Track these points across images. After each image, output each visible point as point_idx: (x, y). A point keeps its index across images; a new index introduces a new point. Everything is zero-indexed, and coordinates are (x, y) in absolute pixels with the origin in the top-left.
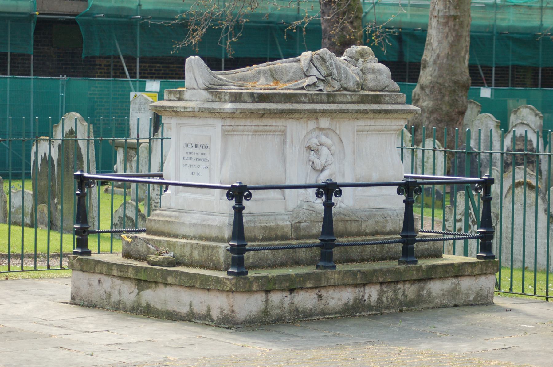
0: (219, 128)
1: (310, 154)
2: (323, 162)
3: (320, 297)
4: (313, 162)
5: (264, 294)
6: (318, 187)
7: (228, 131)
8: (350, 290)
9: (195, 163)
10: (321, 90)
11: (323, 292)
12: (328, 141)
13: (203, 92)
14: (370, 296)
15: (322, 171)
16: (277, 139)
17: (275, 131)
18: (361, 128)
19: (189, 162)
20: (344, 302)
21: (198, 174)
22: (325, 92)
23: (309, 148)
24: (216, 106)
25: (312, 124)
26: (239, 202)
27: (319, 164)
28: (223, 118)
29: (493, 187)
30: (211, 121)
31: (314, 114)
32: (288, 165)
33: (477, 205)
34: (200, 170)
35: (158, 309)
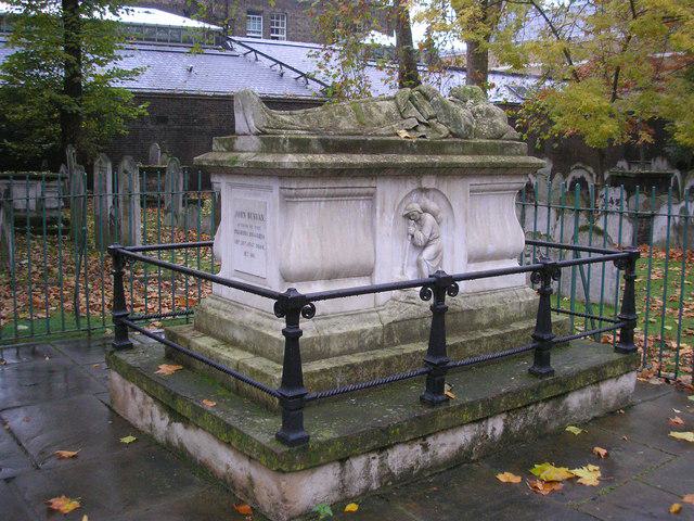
0: (276, 191)
1: (409, 224)
2: (428, 234)
3: (425, 448)
4: (413, 236)
5: (338, 464)
6: (425, 284)
7: (290, 197)
8: (467, 428)
9: (248, 239)
10: (424, 137)
11: (430, 440)
12: (433, 206)
13: (254, 138)
14: (494, 429)
15: (425, 247)
16: (363, 205)
17: (359, 195)
18: (476, 187)
19: (241, 238)
20: (458, 446)
21: (252, 256)
22: (429, 138)
23: (408, 217)
24: (268, 159)
25: (411, 186)
26: (293, 322)
27: (421, 237)
28: (281, 177)
29: (638, 263)
30: (266, 182)
31: (415, 172)
32: (378, 243)
33: (586, 275)
34: (254, 250)
35: (187, 451)
